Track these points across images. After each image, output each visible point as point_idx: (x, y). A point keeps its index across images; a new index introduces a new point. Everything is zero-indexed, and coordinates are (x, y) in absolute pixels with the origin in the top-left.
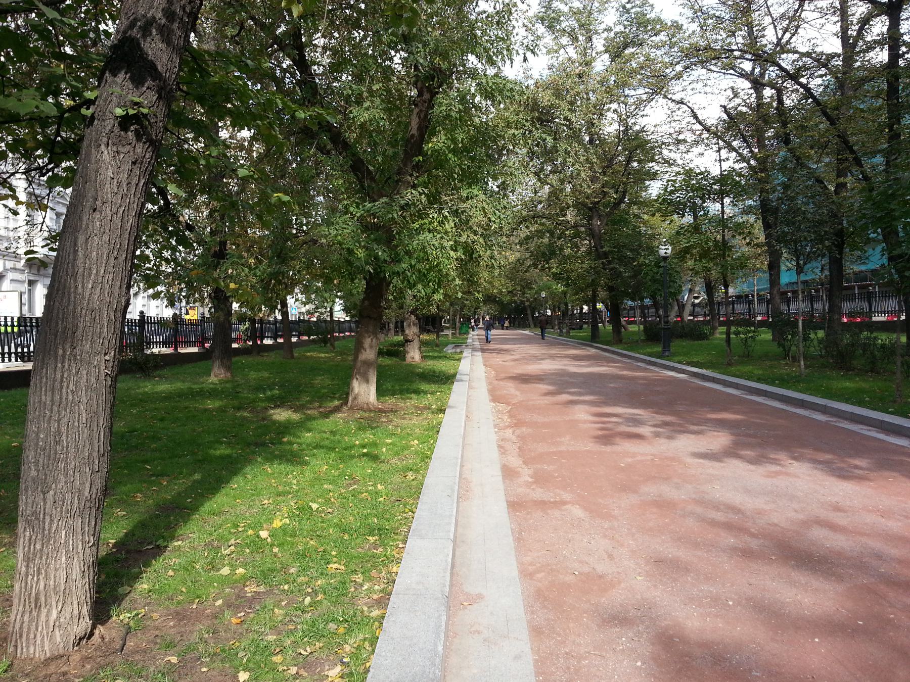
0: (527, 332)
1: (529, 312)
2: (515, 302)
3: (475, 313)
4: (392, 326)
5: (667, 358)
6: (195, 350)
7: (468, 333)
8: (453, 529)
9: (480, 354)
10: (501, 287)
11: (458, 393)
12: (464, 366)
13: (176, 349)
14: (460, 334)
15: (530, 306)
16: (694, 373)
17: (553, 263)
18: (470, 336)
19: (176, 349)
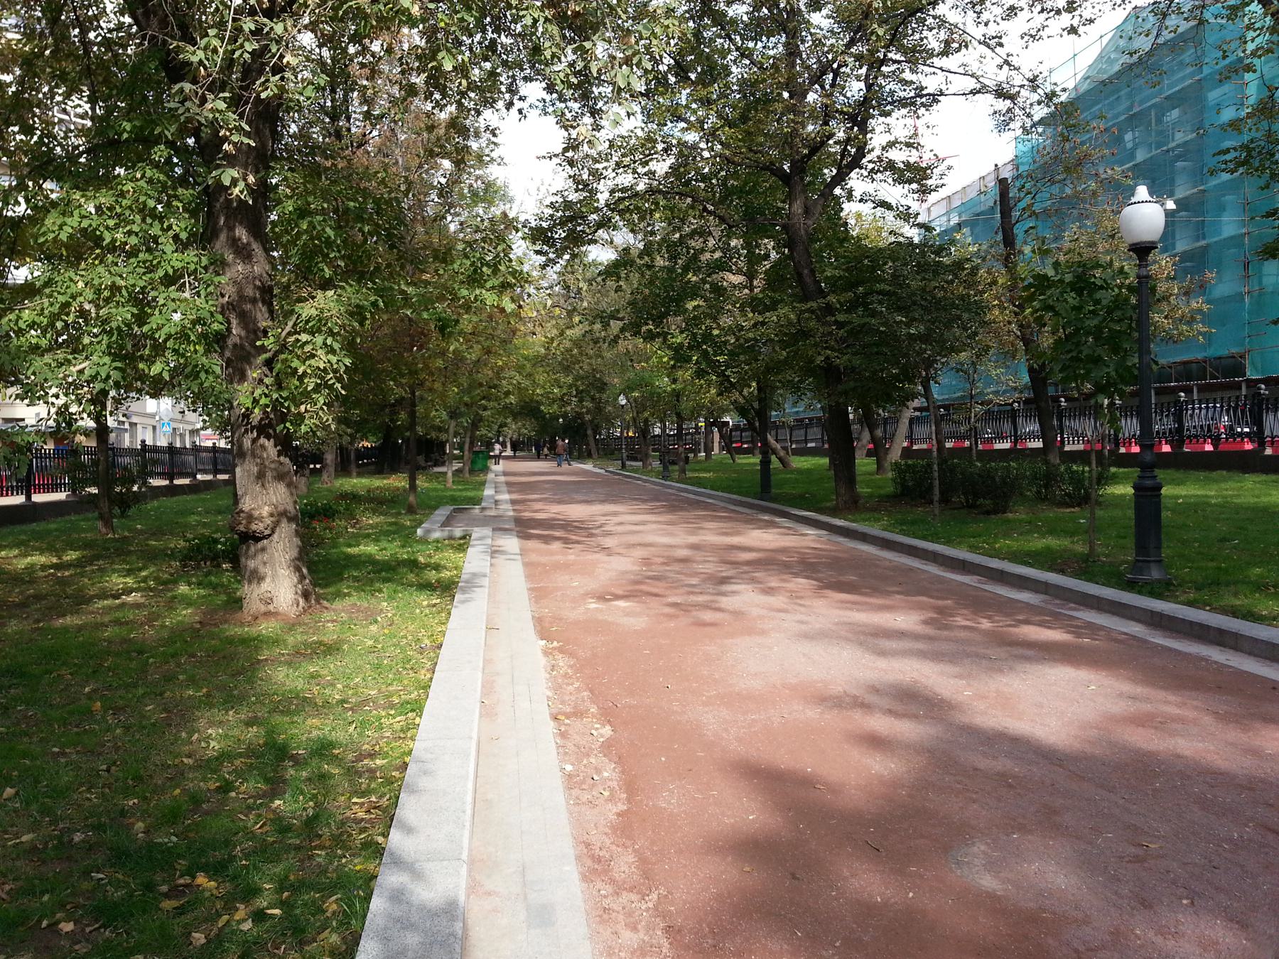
0: (588, 466)
1: (589, 432)
2: (565, 416)
3: (499, 433)
4: (329, 458)
5: (1161, 590)
6: (60, 496)
7: (486, 469)
8: (470, 785)
9: (511, 543)
10: (547, 388)
11: (465, 622)
12: (474, 560)
13: (29, 497)
14: (472, 471)
15: (591, 421)
16: (802, 517)
17: (674, 323)
18: (491, 476)
19: (29, 497)
